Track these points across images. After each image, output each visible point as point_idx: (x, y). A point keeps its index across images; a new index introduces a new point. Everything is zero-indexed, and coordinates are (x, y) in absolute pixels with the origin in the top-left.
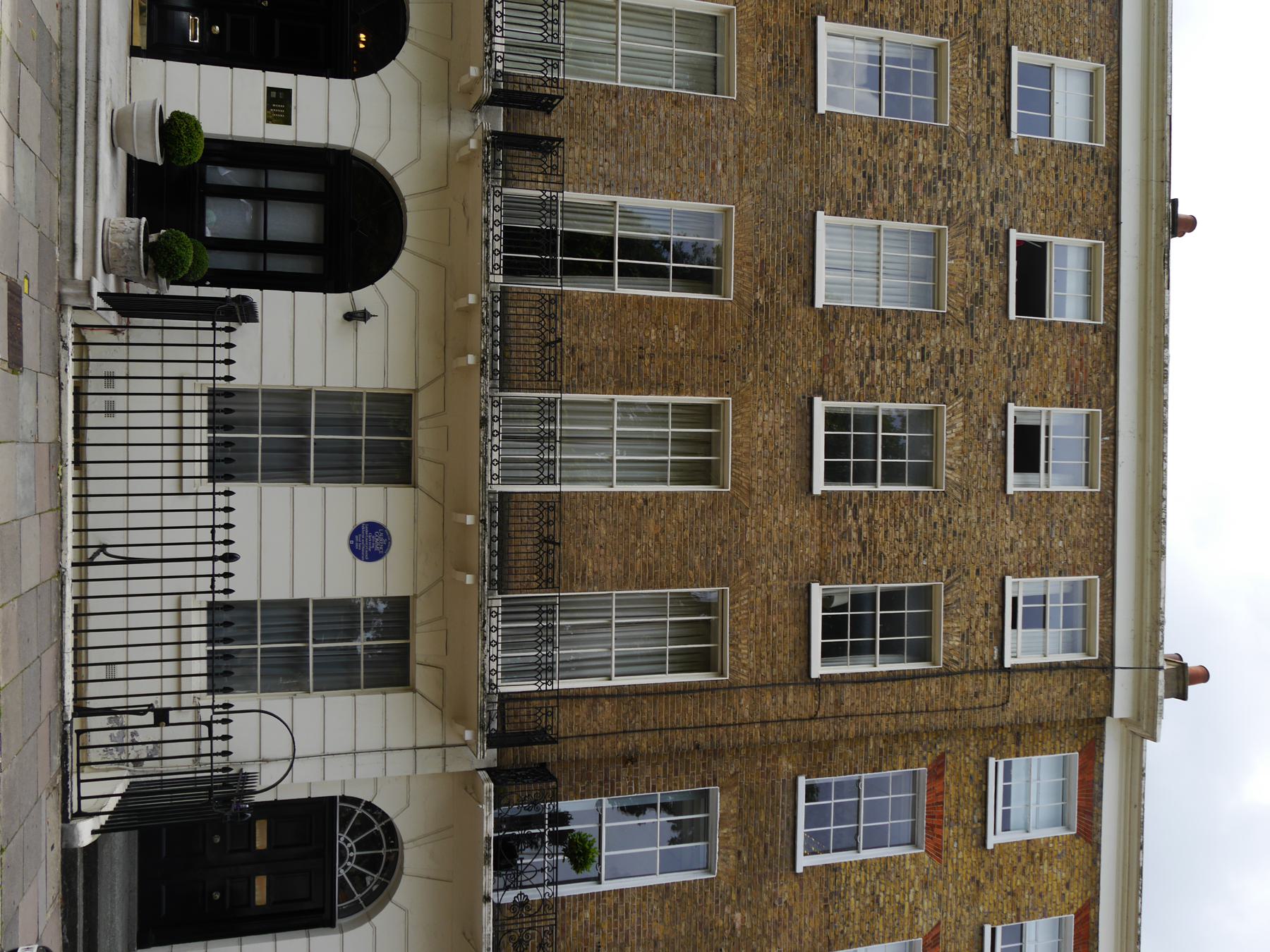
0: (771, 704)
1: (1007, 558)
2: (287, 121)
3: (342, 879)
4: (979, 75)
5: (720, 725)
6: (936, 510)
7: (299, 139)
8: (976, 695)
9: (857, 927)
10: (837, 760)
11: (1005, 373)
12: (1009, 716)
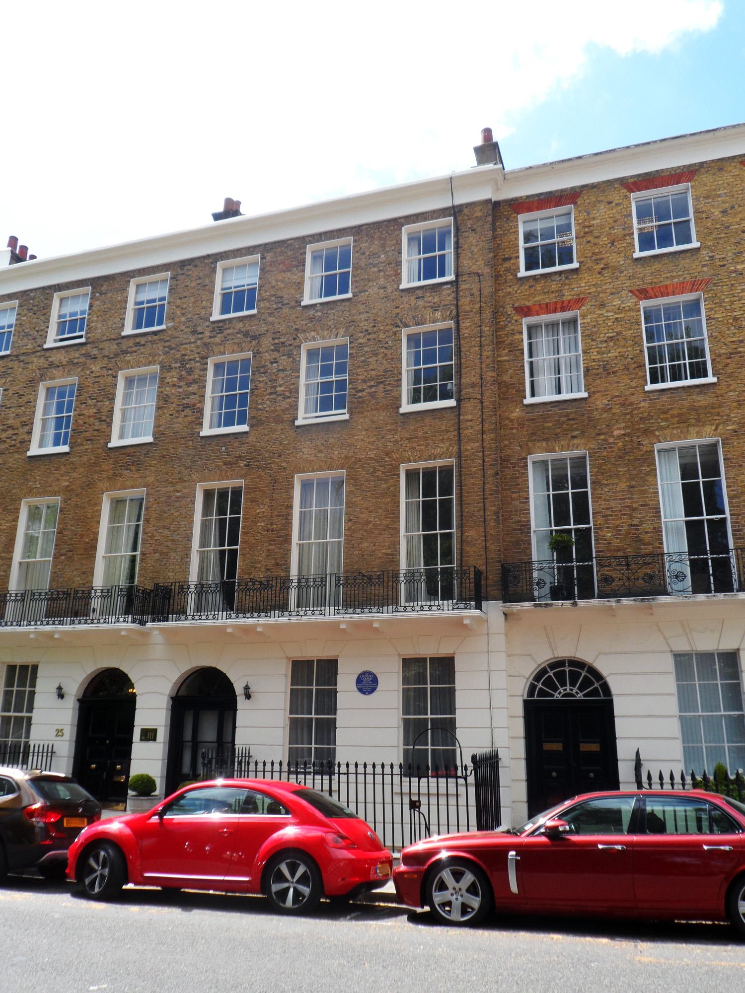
0: (471, 430)
1: (389, 290)
2: (155, 731)
3: (584, 696)
4: (135, 352)
5: (484, 461)
6: (360, 341)
7: (70, 723)
8: (472, 295)
9: (630, 349)
10: (514, 380)
11: (285, 310)
12: (487, 270)
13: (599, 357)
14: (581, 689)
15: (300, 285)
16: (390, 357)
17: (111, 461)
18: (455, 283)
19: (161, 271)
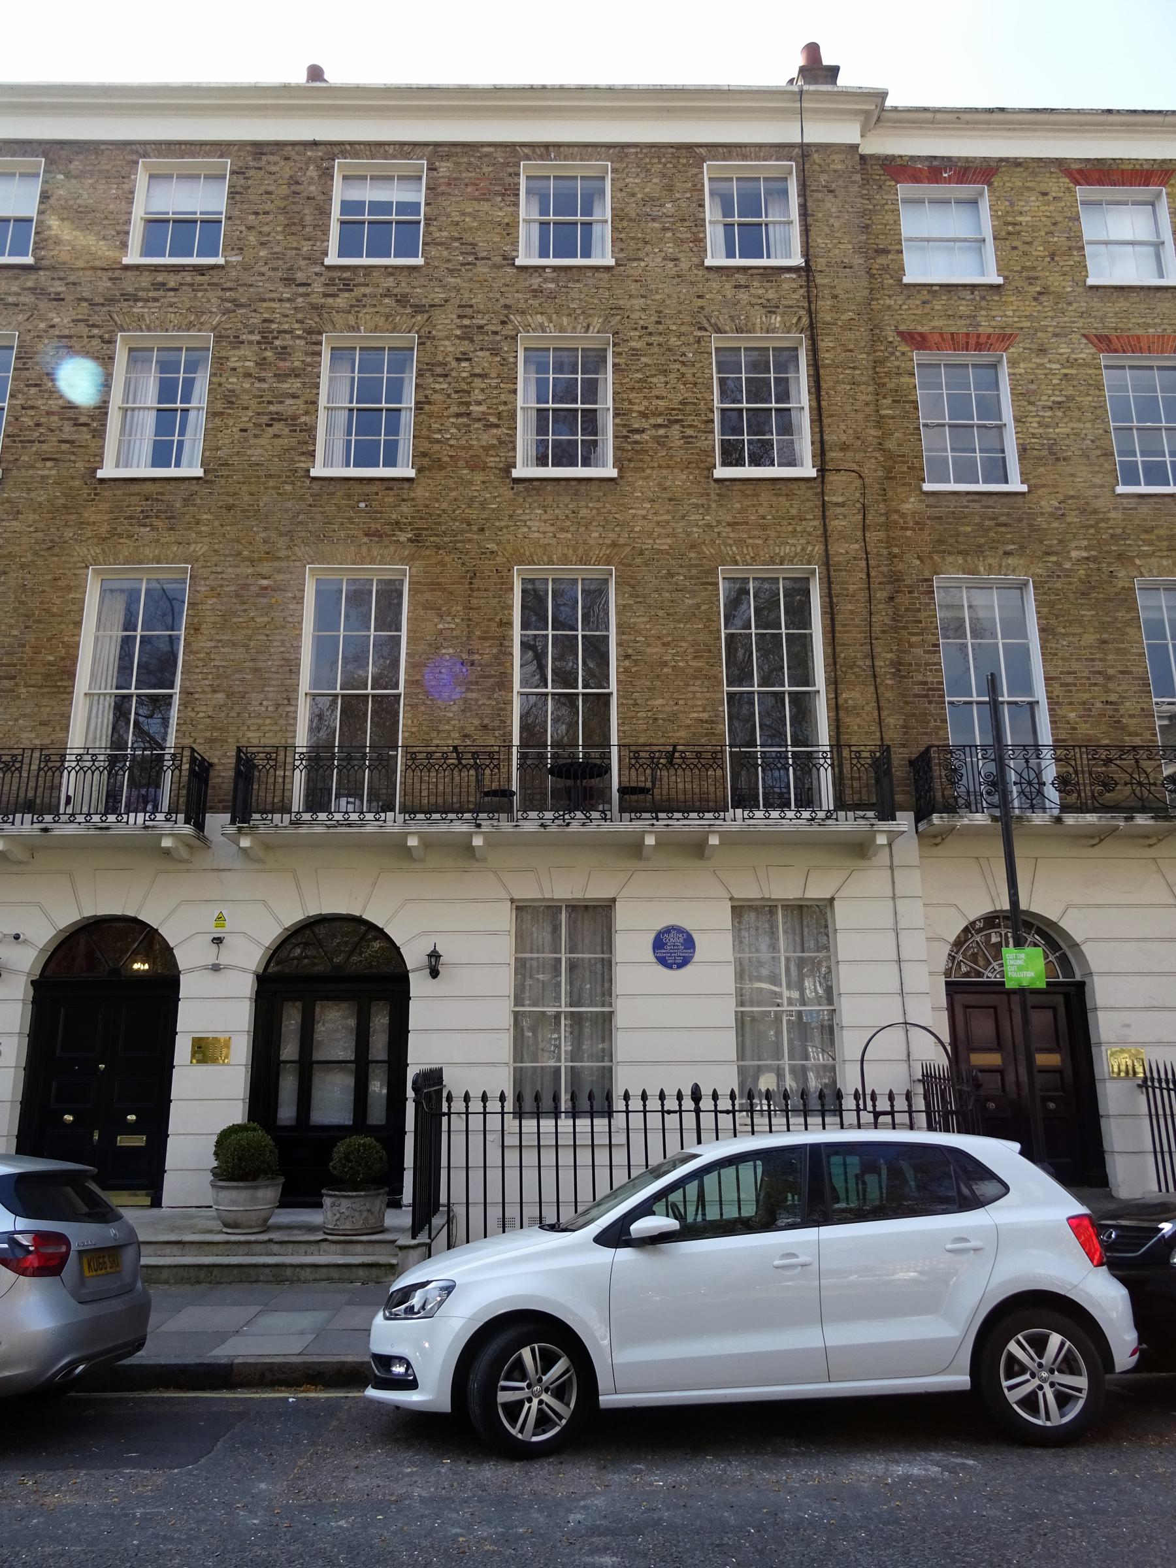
1: (685, 265)
4: (156, 300)
5: (868, 575)
6: (634, 344)
10: (905, 450)
11: (482, 269)
13: (1041, 431)
15: (510, 228)
16: (691, 379)
17: (105, 506)
18: (807, 271)
19: (207, 155)
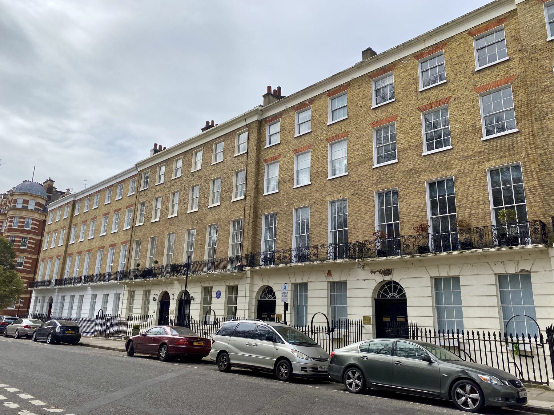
14: (398, 294)
